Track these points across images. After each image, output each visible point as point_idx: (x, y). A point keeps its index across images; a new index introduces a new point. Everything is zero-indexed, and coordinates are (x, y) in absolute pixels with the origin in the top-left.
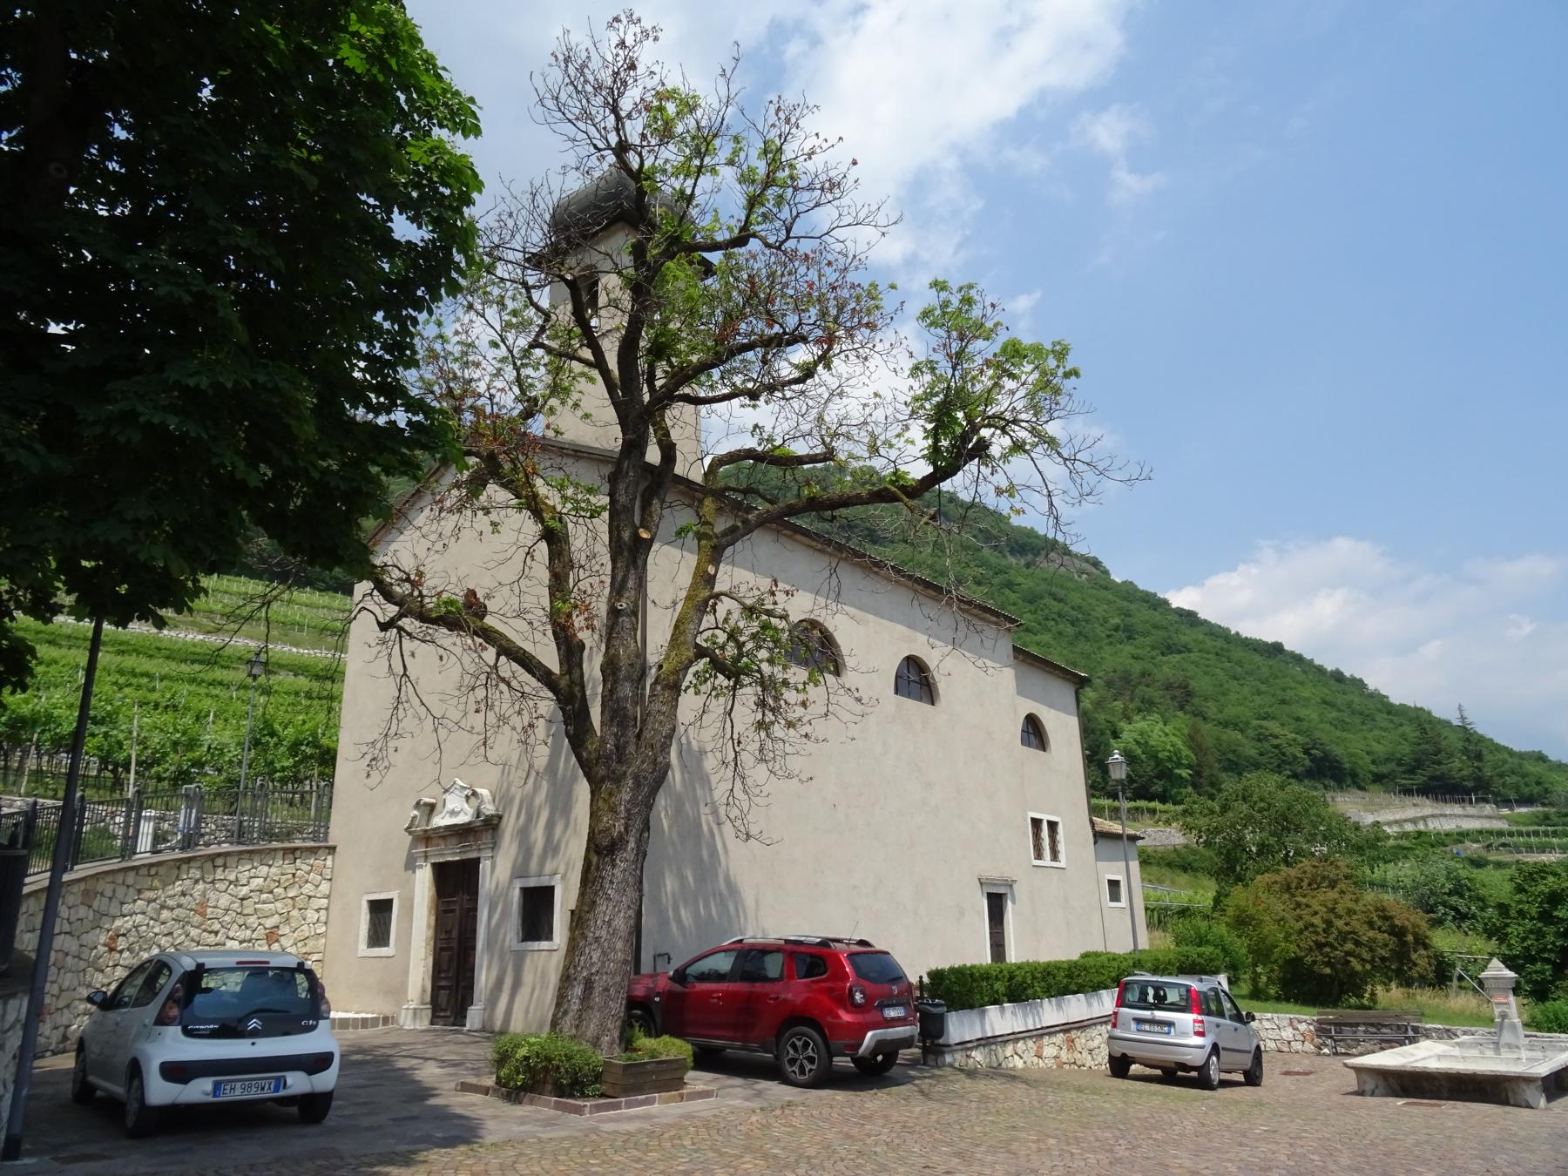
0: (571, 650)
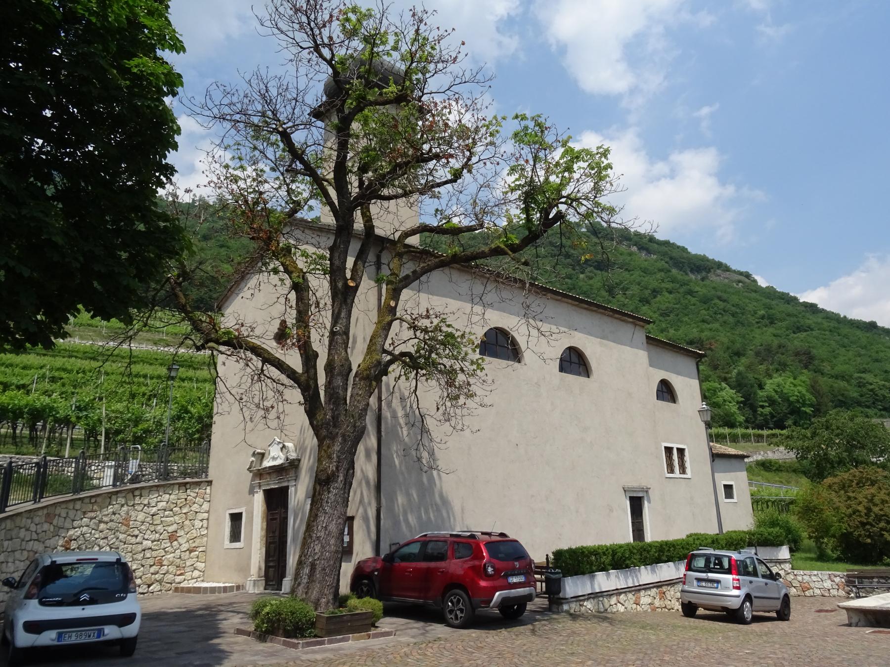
0: (309, 357)
